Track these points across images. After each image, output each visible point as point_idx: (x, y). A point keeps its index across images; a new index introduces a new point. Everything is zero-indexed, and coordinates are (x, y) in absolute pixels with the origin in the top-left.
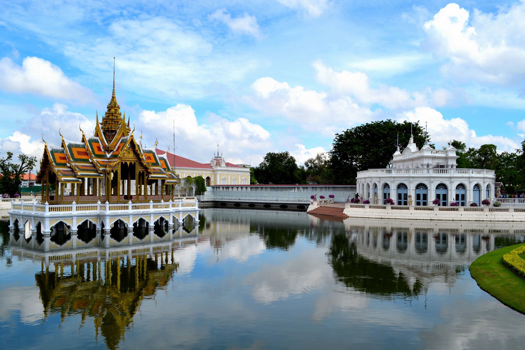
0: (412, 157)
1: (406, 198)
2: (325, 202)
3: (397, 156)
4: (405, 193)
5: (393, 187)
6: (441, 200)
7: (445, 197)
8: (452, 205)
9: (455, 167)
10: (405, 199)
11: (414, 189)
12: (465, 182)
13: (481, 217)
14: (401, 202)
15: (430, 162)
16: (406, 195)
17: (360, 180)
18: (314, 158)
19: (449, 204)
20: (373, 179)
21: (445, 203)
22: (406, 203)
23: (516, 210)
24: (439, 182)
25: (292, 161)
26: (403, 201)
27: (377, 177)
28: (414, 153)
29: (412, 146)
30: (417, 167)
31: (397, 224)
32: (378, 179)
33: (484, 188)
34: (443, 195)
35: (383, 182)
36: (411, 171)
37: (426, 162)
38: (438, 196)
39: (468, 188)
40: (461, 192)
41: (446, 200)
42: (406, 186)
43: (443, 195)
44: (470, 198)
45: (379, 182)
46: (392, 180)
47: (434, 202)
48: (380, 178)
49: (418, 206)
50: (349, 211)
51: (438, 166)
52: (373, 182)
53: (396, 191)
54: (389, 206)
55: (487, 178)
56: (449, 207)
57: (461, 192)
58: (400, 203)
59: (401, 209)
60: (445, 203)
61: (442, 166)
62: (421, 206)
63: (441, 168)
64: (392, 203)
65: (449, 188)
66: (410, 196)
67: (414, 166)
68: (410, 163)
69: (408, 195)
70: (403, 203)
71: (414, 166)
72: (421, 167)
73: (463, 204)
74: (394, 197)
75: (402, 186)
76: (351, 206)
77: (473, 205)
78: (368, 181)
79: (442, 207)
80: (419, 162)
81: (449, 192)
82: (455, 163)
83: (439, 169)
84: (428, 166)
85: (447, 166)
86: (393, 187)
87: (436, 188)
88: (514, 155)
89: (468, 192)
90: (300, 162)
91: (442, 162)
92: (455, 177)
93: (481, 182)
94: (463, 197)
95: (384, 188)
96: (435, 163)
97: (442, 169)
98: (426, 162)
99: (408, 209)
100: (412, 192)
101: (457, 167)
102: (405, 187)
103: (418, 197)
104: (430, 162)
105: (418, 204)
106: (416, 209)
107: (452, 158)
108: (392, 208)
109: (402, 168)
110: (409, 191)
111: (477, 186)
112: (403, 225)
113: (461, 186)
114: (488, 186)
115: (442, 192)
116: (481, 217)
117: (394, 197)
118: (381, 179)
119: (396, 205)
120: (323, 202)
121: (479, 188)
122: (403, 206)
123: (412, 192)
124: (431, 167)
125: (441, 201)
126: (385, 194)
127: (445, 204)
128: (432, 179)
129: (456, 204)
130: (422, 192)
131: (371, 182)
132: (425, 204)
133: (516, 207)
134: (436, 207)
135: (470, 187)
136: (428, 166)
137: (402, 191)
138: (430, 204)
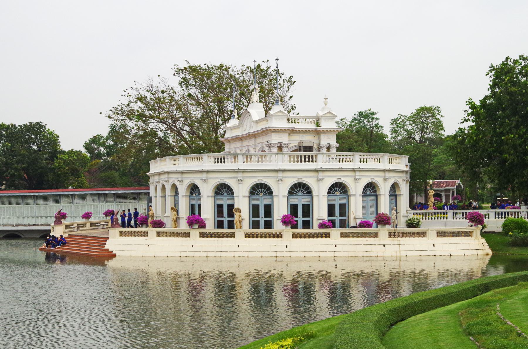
0: (255, 129)
1: (231, 214)
2: (92, 224)
3: (232, 129)
4: (230, 203)
5: (207, 191)
6: (299, 218)
7: (307, 210)
8: (322, 225)
9: (333, 150)
10: (341, 215)
11: (286, 194)
12: (347, 180)
13: (373, 248)
14: (222, 221)
15: (284, 139)
16: (231, 207)
17: (156, 178)
18: (105, 134)
19: (316, 224)
20: (171, 176)
21: (270, 221)
22: (231, 225)
23: (441, 234)
24: (333, 181)
25: (52, 141)
26: (226, 219)
27: (177, 172)
28: (257, 122)
29: (256, 109)
30: (263, 151)
31: (209, 268)
32: (179, 176)
33: (384, 189)
34: (303, 206)
35: (188, 180)
36: (255, 159)
37: (275, 139)
38: (294, 209)
39: (352, 191)
40: (338, 200)
41: (218, 221)
42: (269, 189)
43: (303, 206)
44: (357, 210)
45: (181, 181)
46: (204, 176)
47: (286, 221)
48: (182, 173)
49: (220, 230)
50: (117, 242)
51: (300, 148)
52: (171, 182)
53: (326, 199)
54: (195, 231)
55: (390, 171)
56: (315, 229)
57: (338, 200)
58: (220, 224)
59: (223, 236)
60: (270, 221)
61: (309, 149)
62: (262, 230)
63: (306, 152)
64: (202, 225)
65: (315, 192)
66: (239, 210)
67: (258, 148)
68: (251, 142)
69: (236, 207)
70: (226, 224)
71: (258, 148)
72: (266, 149)
73: (343, 224)
74: (208, 213)
75: (223, 189)
76: (122, 234)
77: (365, 224)
78: (174, 179)
79: (300, 230)
80: (262, 141)
81: (315, 199)
82: (332, 141)
83: (303, 153)
84: (280, 147)
85: (319, 148)
86: (207, 191)
87: (329, 193)
88: (462, 131)
89: (352, 199)
90: (72, 140)
91: (308, 140)
92: (330, 167)
93: (379, 180)
94: (343, 208)
95: (191, 193)
96: (295, 140)
97: (307, 154)
98: (275, 139)
99: (233, 235)
100: (242, 203)
101: (338, 150)
102: (267, 190)
103: (255, 210)
104: (284, 139)
105: (256, 225)
106: (248, 236)
107: (328, 131)
108: (202, 235)
109: (238, 152)
110: (236, 199)
111: (371, 188)
112: (227, 268)
113: (339, 188)
114: (394, 187)
115: (300, 200)
116: (373, 248)
117: (208, 213)
118: (185, 176)
119: (210, 227)
120: (88, 225)
121: (375, 191)
122: (226, 230)
123: (242, 203)
124: (285, 150)
125: (300, 219)
126: (192, 207)
127: (307, 224)
128: (280, 174)
129: (332, 224)
130: (261, 201)
131: (167, 181)
132: (268, 225)
133: (442, 228)
134: (288, 232)
135: (356, 189)
136: (280, 147)
137: (224, 201)
138: (278, 226)
